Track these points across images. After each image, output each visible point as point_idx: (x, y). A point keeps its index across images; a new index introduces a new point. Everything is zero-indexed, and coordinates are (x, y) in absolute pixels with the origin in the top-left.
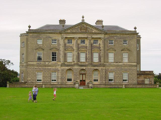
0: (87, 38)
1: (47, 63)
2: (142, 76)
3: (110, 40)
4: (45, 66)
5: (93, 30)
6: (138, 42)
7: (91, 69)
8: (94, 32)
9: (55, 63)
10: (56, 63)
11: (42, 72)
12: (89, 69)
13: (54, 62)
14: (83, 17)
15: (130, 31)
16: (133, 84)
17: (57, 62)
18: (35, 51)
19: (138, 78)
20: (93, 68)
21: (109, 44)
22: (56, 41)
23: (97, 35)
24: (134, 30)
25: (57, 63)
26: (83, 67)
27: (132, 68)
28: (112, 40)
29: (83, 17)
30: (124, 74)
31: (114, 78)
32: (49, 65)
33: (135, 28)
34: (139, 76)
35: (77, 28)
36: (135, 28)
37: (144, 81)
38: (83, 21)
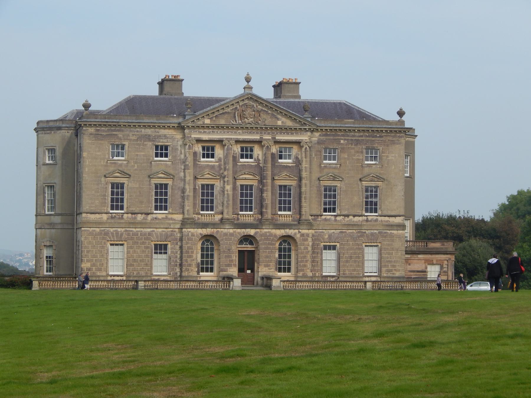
0: (259, 142)
1: (140, 217)
2: (420, 256)
3: (325, 149)
4: (134, 224)
5: (279, 117)
6: (410, 151)
7: (194, 236)
8: (279, 123)
9: (164, 216)
10: (167, 218)
11: (125, 243)
12: (265, 235)
13: (160, 214)
14: (248, 80)
15: (387, 122)
16: (395, 280)
17: (169, 213)
18: (103, 179)
19: (407, 260)
20: (239, 230)
21: (204, 157)
22: (335, 153)
23: (228, 132)
24: (397, 118)
25: (170, 216)
26: (248, 230)
27: (392, 231)
28: (335, 150)
29: (248, 80)
30: (367, 250)
31: (152, 258)
32: (145, 223)
33: (401, 113)
34: (409, 256)
35: (228, 110)
36: (401, 113)
37: (425, 272)
38: (248, 91)
